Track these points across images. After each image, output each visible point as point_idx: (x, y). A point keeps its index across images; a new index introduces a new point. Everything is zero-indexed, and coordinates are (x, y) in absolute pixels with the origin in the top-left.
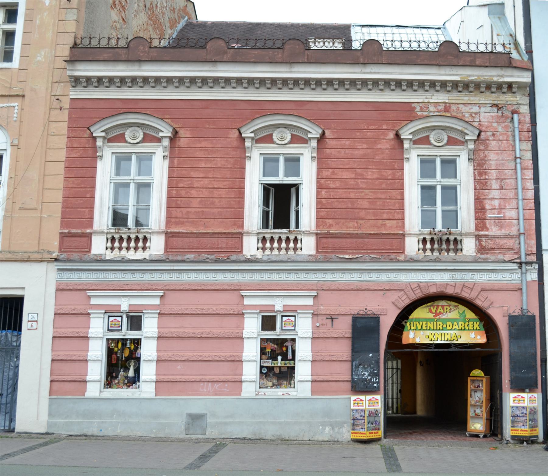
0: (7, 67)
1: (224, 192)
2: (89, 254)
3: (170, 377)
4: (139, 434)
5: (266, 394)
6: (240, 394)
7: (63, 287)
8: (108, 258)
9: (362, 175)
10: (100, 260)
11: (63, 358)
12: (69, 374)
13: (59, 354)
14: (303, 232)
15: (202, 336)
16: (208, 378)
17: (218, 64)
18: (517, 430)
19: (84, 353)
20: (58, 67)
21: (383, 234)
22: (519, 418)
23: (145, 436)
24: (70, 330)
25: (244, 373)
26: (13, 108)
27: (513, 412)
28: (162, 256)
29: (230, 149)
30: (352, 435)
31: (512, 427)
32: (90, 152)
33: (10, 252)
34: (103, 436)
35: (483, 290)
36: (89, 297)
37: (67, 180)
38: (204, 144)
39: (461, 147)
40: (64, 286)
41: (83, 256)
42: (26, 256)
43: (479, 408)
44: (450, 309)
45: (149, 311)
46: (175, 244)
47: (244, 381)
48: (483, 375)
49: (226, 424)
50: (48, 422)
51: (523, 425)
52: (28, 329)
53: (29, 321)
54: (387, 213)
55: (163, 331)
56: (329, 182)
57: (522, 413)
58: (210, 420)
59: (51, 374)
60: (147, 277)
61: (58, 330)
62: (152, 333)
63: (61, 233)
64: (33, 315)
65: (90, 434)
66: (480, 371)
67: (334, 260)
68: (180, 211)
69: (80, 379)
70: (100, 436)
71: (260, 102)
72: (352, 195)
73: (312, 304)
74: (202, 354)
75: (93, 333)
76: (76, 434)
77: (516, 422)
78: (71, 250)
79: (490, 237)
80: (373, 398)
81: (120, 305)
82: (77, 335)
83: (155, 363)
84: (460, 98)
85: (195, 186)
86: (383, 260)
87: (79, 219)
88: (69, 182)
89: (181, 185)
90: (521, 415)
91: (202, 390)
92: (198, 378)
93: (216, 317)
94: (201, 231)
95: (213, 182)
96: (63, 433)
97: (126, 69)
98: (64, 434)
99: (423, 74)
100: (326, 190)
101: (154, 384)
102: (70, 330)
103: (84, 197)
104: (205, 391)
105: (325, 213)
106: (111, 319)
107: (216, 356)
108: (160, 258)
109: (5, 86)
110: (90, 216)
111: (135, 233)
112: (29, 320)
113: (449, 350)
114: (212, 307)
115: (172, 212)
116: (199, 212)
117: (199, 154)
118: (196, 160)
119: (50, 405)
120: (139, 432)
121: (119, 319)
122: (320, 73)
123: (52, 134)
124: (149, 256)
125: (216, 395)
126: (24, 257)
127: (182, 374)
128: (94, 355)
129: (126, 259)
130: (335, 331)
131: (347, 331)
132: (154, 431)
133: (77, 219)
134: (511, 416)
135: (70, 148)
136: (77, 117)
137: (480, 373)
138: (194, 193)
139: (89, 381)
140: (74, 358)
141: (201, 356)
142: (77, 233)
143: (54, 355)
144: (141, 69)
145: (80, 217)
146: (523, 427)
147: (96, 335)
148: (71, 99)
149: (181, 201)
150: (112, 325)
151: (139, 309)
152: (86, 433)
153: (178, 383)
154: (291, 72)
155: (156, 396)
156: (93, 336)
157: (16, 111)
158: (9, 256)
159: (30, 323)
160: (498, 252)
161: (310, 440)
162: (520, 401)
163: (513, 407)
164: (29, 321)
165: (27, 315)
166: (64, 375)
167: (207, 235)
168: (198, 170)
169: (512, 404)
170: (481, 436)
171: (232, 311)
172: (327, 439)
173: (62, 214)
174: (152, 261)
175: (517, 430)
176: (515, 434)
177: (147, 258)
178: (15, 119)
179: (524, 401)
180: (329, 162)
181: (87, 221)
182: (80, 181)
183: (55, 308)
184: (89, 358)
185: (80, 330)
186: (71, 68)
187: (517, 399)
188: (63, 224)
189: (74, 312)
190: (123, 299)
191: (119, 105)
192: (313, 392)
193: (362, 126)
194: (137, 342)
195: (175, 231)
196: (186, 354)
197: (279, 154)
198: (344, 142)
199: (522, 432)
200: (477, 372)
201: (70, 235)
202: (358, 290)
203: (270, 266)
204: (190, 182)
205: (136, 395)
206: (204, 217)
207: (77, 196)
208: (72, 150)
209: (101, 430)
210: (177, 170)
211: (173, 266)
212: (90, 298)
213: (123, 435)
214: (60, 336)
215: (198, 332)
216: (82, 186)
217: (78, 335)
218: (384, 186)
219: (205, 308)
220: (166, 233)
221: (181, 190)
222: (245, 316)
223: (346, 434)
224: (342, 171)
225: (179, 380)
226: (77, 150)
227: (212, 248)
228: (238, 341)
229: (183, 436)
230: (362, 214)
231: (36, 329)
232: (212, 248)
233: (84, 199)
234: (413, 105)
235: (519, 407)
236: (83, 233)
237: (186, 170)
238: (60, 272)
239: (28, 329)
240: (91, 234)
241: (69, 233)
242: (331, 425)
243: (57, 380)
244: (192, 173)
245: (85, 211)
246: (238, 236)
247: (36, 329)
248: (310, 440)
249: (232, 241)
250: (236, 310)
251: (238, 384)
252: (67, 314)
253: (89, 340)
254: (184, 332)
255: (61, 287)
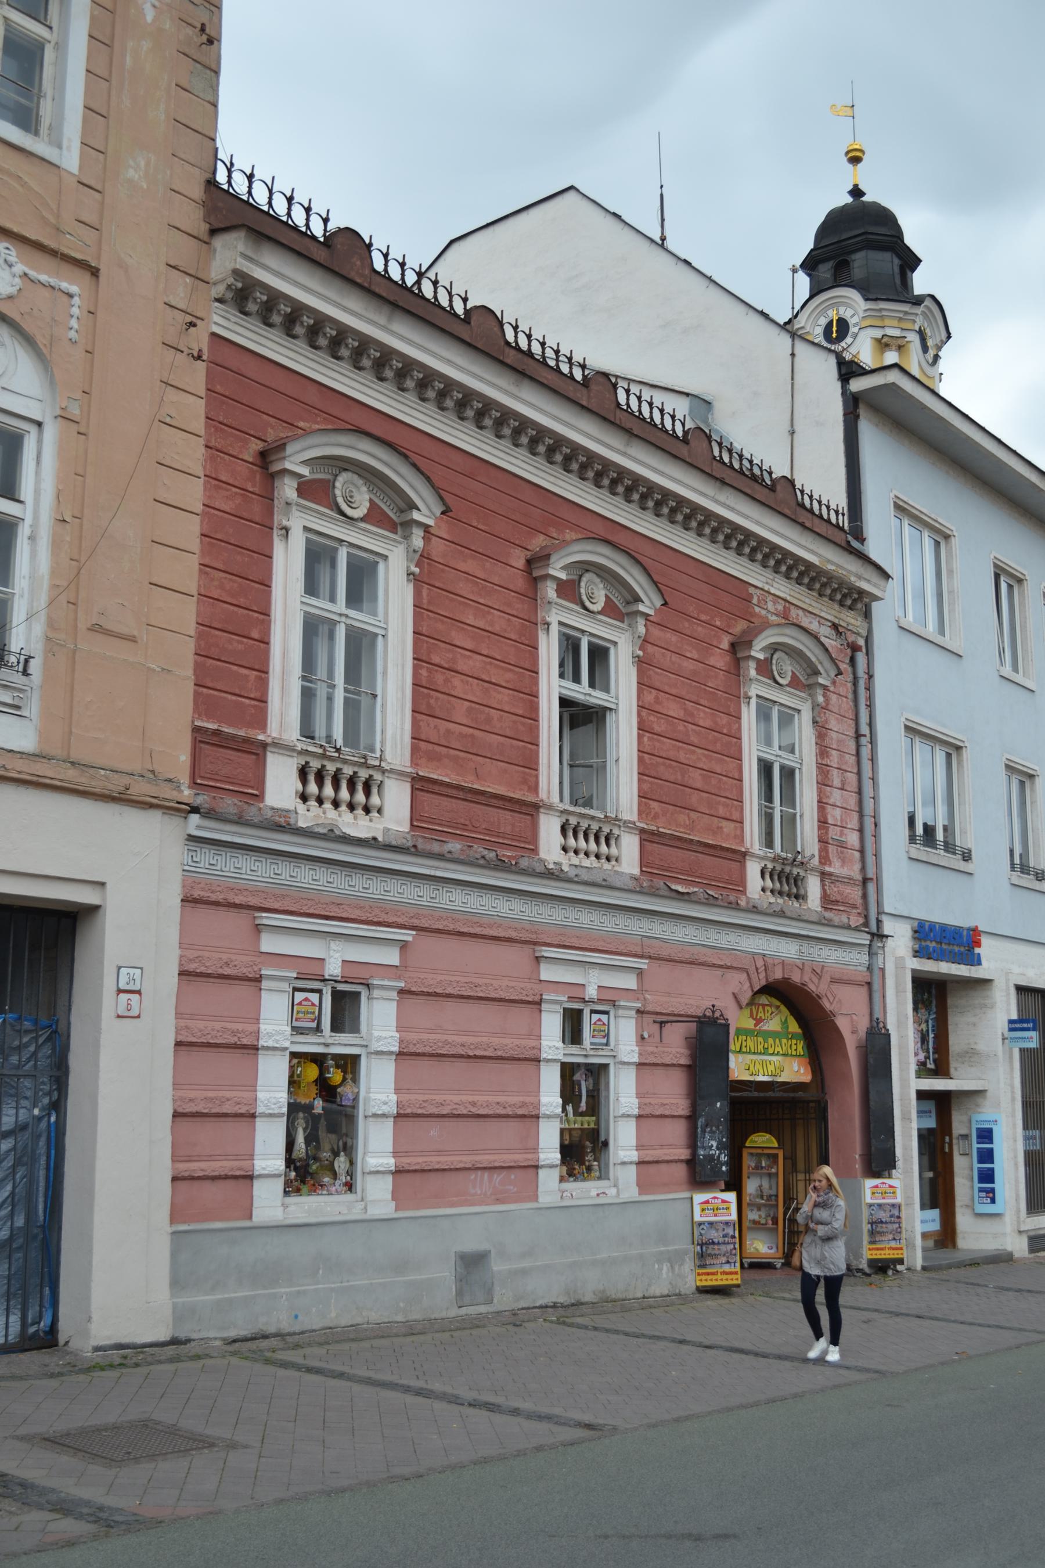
0: (47, 158)
1: (506, 699)
2: (261, 805)
3: (420, 1160)
4: (374, 1316)
5: (574, 1194)
6: (535, 1198)
7: (202, 894)
8: (302, 824)
9: (692, 715)
10: (282, 825)
11: (201, 1108)
12: (211, 1158)
13: (192, 1094)
14: (625, 822)
15: (477, 1054)
16: (485, 1159)
17: (526, 382)
18: (882, 1249)
19: (246, 1095)
20: (178, 225)
21: (722, 848)
22: (884, 1225)
23: (386, 1320)
24: (218, 1025)
25: (541, 1145)
26: (65, 298)
27: (871, 1214)
28: (407, 836)
29: (513, 594)
30: (698, 1278)
31: (871, 1242)
32: (256, 509)
33: (73, 763)
34: (302, 1333)
35: (834, 981)
36: (258, 929)
37: (206, 573)
38: (470, 565)
39: (802, 694)
40: (203, 889)
41: (246, 806)
42: (115, 784)
43: (755, 1209)
44: (772, 1013)
45: (386, 983)
46: (427, 808)
47: (543, 1166)
48: (776, 1145)
49: (524, 1272)
50: (175, 1306)
51: (894, 1239)
52: (119, 1016)
53: (120, 991)
54: (726, 805)
55: (413, 1037)
56: (652, 718)
57: (891, 1216)
58: (498, 1266)
59: (175, 1159)
60: (377, 889)
61: (191, 1023)
62: (389, 1040)
63: (196, 730)
64: (132, 971)
65: (272, 1330)
66: (768, 1136)
67: (661, 893)
68: (436, 727)
69: (240, 1169)
70: (295, 1334)
71: (555, 498)
72: (682, 757)
73: (635, 987)
74: (475, 1098)
75: (270, 1035)
76: (243, 1333)
77: (879, 1233)
78: (218, 785)
79: (833, 878)
80: (715, 1198)
81: (324, 959)
82: (233, 1040)
83: (390, 1123)
84: (803, 598)
85: (459, 669)
86: (720, 903)
87: (234, 698)
88: (212, 580)
89: (436, 659)
90: (888, 1220)
91: (473, 1191)
92: (467, 1160)
93: (496, 1007)
94: (475, 786)
95: (488, 667)
96: (212, 1335)
97: (364, 313)
98: (216, 1339)
99: (782, 536)
100: (651, 735)
101: (389, 1179)
102: (218, 1025)
103: (246, 633)
104: (479, 1192)
105: (649, 785)
106: (299, 996)
107: (498, 1103)
108: (404, 841)
109: (43, 217)
110: (257, 695)
111: (355, 764)
112: (122, 986)
113: (770, 1094)
114: (493, 982)
115: (421, 723)
116: (466, 736)
117: (464, 588)
118: (461, 603)
119: (174, 1254)
120: (376, 1314)
121: (314, 998)
122: (662, 474)
123: (168, 420)
124: (384, 835)
125: (499, 1201)
126: (111, 787)
127: (439, 1152)
128: (274, 1101)
129: (337, 832)
130: (666, 1049)
131: (678, 1050)
132: (402, 1305)
133: (229, 697)
134: (869, 1223)
135: (212, 479)
136: (227, 394)
137: (768, 1141)
138: (458, 684)
139: (260, 1176)
140: (227, 1108)
141: (474, 1104)
142: (233, 737)
143: (182, 1099)
144: (390, 327)
145: (237, 691)
146: (894, 1242)
147: (277, 1041)
148: (214, 335)
149: (437, 699)
150: (301, 1015)
151: (362, 973)
152: (264, 1328)
153: (432, 1175)
154: (624, 454)
155: (396, 1210)
156: (270, 1043)
157: (75, 311)
158: (70, 775)
159: (124, 997)
160: (842, 908)
161: (644, 1297)
162: (885, 1193)
163: (870, 1205)
164: (120, 991)
165: (115, 970)
166: (199, 1159)
167: (480, 797)
168: (463, 629)
169: (868, 1200)
170: (779, 1266)
171: (525, 993)
172: (666, 1292)
173: (195, 671)
174: (389, 847)
175: (882, 1249)
176: (879, 1257)
177: (380, 839)
178: (72, 334)
179: (894, 1193)
180: (651, 672)
181: (254, 706)
182: (236, 585)
183: (181, 956)
184: (260, 1109)
185: (240, 1027)
186: (249, 253)
187: (879, 1190)
188: (203, 705)
189: (227, 971)
190: (335, 945)
191: (312, 396)
192: (643, 1185)
193: (691, 610)
194: (349, 1064)
195: (432, 776)
196: (449, 1098)
197: (583, 632)
198: (668, 635)
199: (892, 1252)
200: (301, 1115)
201: (215, 740)
202: (693, 963)
203: (589, 893)
204: (450, 656)
205: (356, 1213)
206: (474, 751)
207: (230, 629)
208: (217, 487)
209: (296, 1317)
210: (428, 615)
211: (437, 868)
212: (259, 932)
213: (343, 1323)
214: (194, 1040)
215: (471, 1042)
216: (242, 601)
217: (236, 1039)
218: (718, 747)
219: (480, 981)
220: (413, 779)
221: (437, 671)
222: (265, 984)
223: (689, 1279)
224: (668, 699)
225: (437, 1167)
226: (227, 490)
227: (488, 831)
228: (530, 1067)
229: (454, 1312)
230: (694, 798)
231: (138, 1017)
232: (488, 831)
233: (245, 640)
234: (751, 590)
235: (885, 1204)
236: (246, 740)
237: (442, 621)
238: (192, 845)
239: (119, 1016)
240: (264, 745)
241: (216, 733)
242: (669, 1261)
243: (186, 1174)
244: (453, 634)
245: (247, 676)
246: (530, 810)
247: (138, 1017)
248: (644, 1297)
249: (520, 822)
250: (531, 992)
251: (532, 1171)
252: (209, 975)
253: (256, 1055)
254: (446, 1043)
255: (197, 894)
